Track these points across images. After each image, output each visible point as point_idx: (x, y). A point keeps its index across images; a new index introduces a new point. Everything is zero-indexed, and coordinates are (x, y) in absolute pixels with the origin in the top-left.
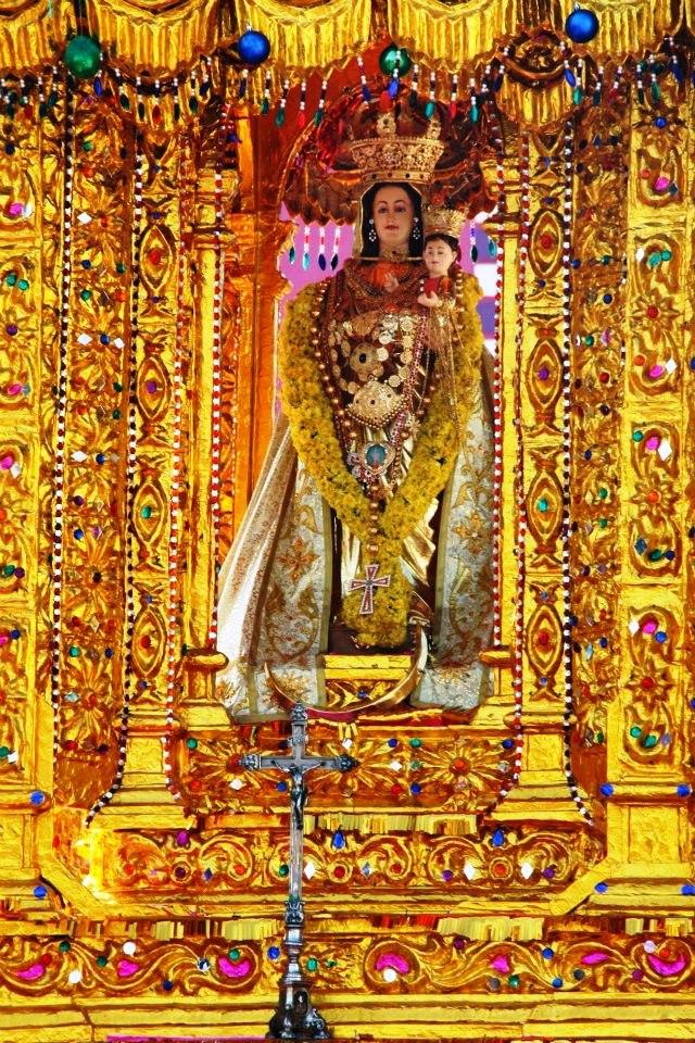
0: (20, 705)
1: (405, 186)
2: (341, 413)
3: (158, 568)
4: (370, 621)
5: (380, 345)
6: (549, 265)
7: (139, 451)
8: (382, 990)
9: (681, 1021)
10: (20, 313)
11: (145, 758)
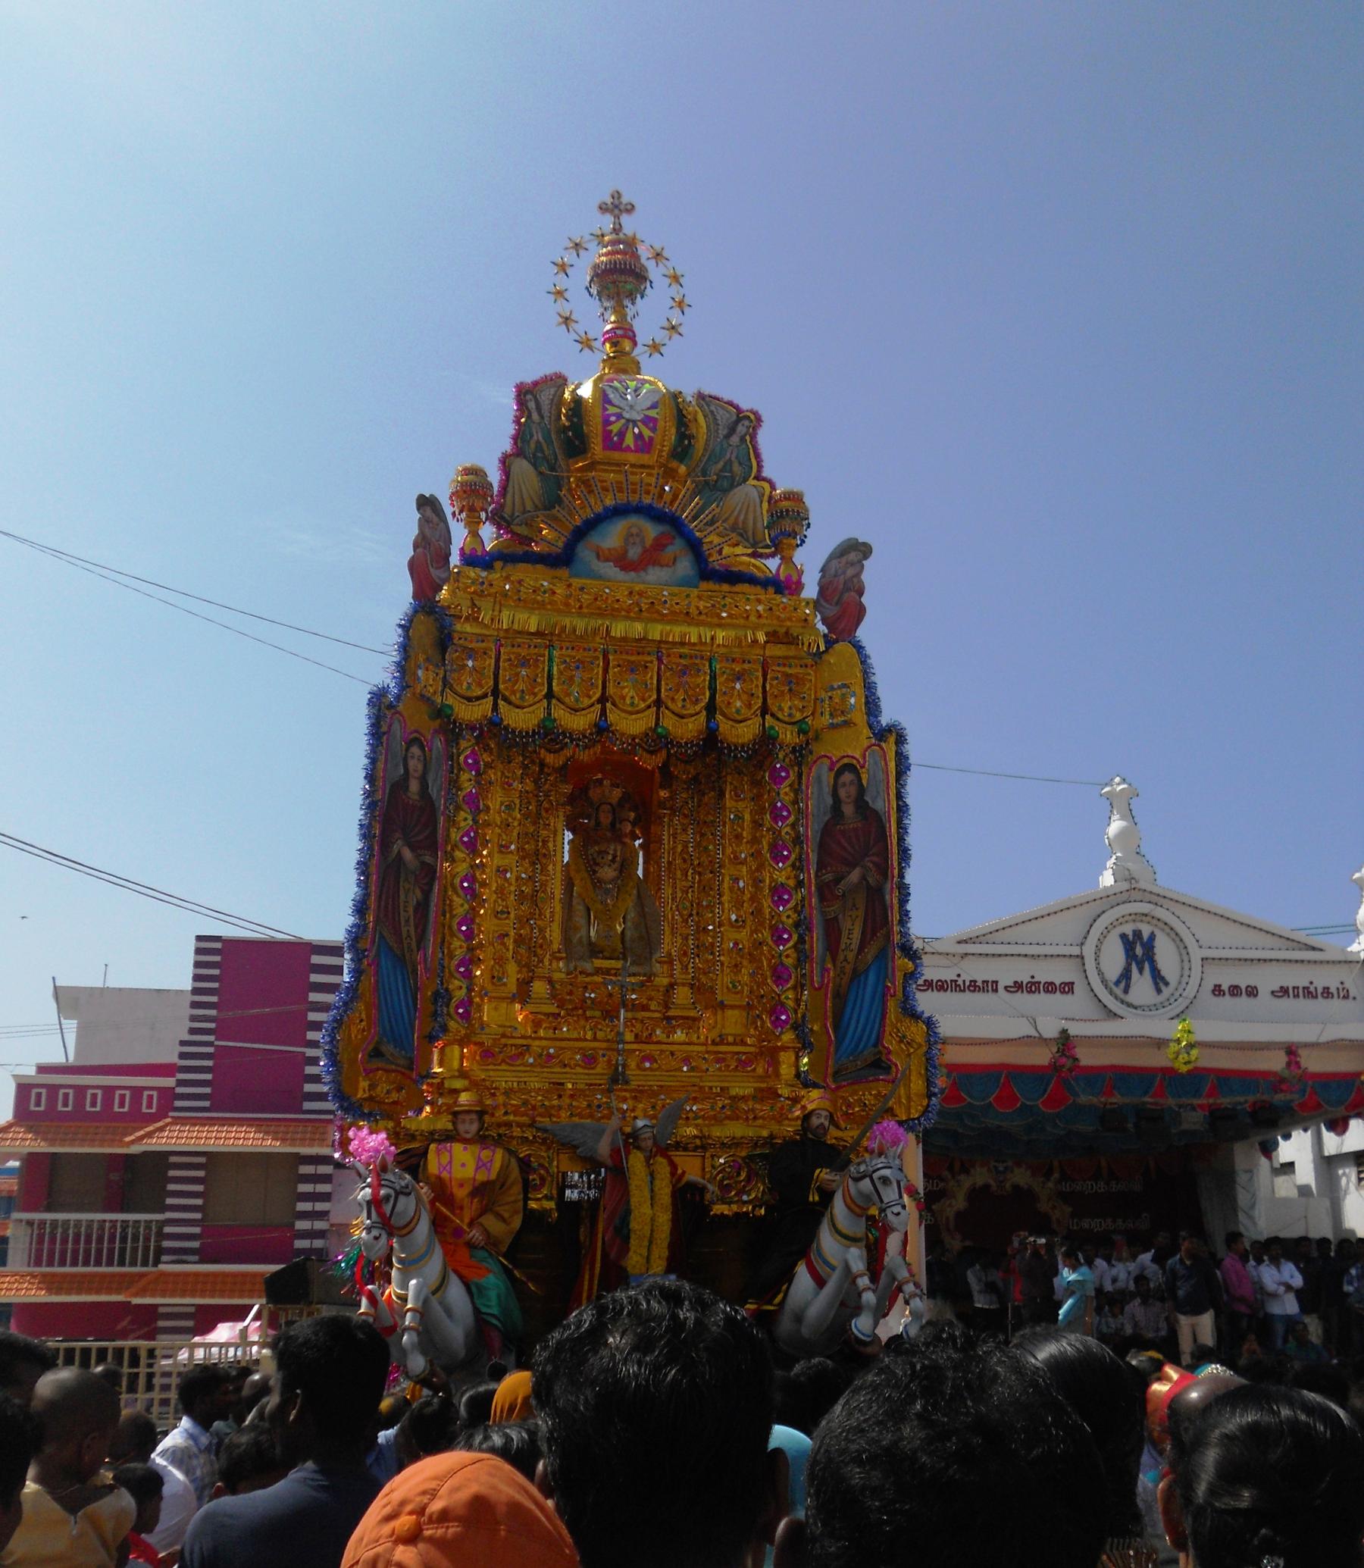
1: (610, 804)
8: (645, 1069)
9: (1018, 987)
10: (510, 820)
11: (539, 988)
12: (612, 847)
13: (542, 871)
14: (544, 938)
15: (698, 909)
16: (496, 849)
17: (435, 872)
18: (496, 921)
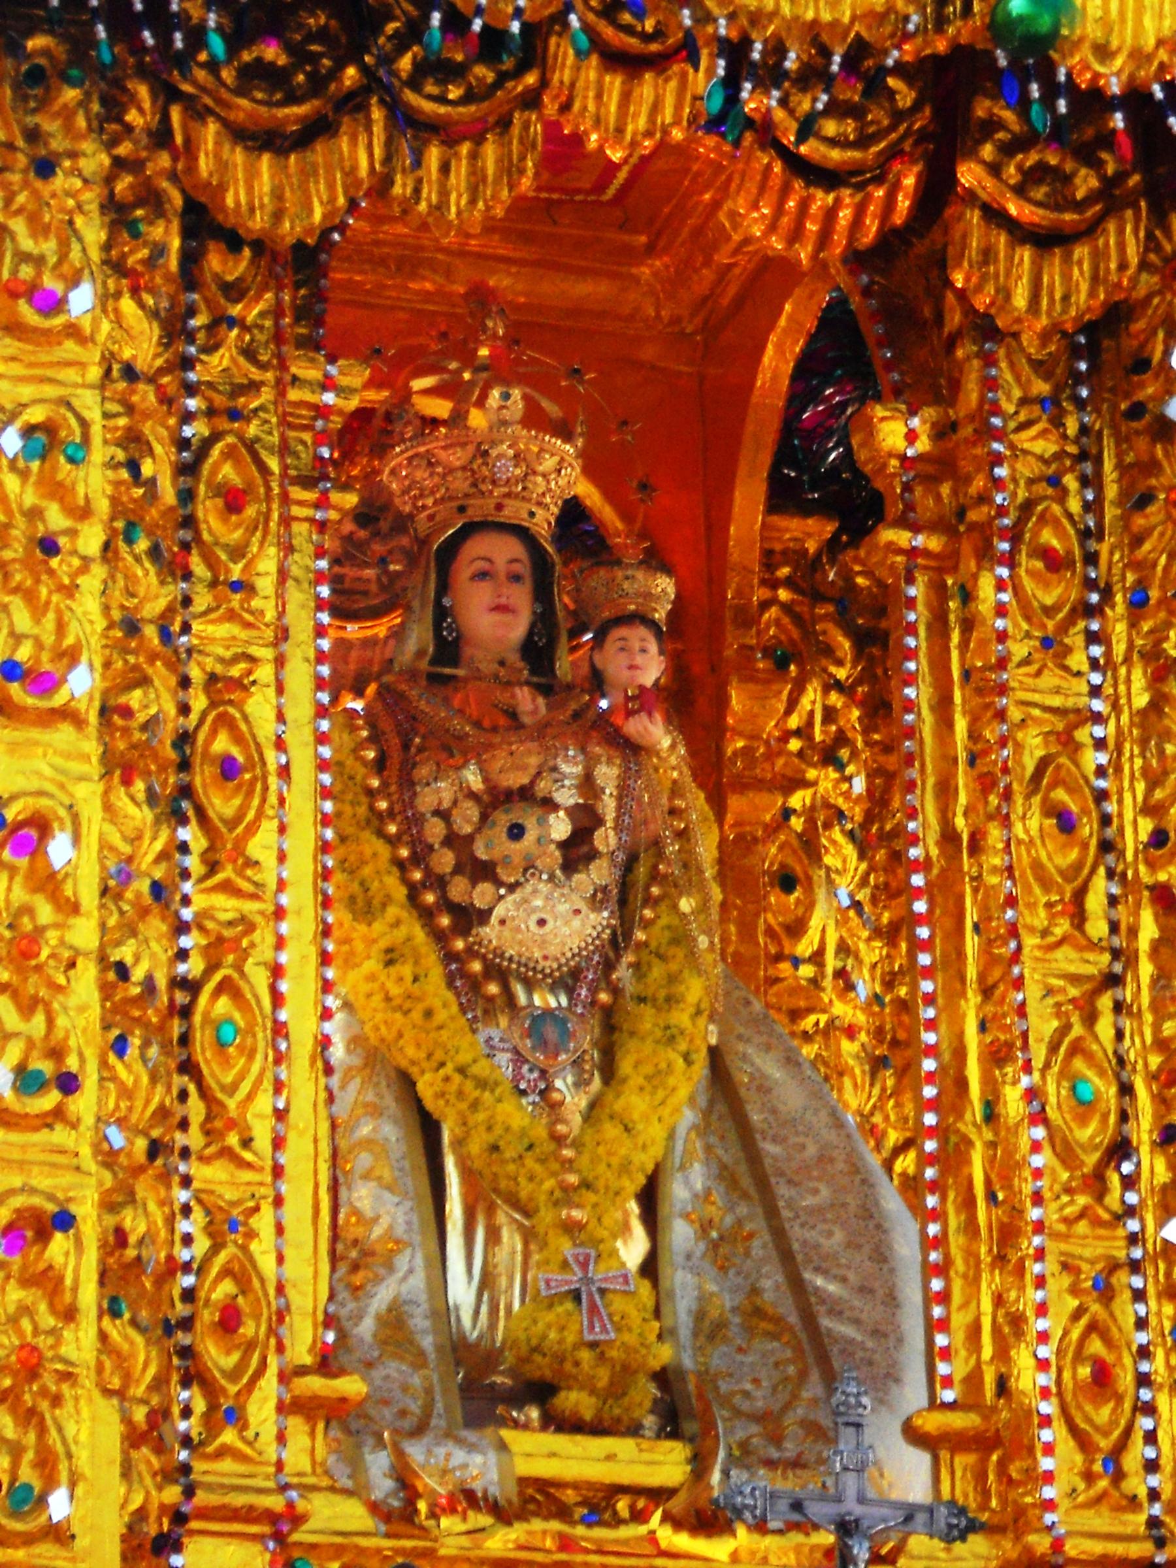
0: (65, 1388)
1: (522, 533)
2: (460, 945)
4: (602, 1357)
5: (555, 807)
6: (220, 990)
7: (200, 901)
12: (571, 769)
13: (212, 867)
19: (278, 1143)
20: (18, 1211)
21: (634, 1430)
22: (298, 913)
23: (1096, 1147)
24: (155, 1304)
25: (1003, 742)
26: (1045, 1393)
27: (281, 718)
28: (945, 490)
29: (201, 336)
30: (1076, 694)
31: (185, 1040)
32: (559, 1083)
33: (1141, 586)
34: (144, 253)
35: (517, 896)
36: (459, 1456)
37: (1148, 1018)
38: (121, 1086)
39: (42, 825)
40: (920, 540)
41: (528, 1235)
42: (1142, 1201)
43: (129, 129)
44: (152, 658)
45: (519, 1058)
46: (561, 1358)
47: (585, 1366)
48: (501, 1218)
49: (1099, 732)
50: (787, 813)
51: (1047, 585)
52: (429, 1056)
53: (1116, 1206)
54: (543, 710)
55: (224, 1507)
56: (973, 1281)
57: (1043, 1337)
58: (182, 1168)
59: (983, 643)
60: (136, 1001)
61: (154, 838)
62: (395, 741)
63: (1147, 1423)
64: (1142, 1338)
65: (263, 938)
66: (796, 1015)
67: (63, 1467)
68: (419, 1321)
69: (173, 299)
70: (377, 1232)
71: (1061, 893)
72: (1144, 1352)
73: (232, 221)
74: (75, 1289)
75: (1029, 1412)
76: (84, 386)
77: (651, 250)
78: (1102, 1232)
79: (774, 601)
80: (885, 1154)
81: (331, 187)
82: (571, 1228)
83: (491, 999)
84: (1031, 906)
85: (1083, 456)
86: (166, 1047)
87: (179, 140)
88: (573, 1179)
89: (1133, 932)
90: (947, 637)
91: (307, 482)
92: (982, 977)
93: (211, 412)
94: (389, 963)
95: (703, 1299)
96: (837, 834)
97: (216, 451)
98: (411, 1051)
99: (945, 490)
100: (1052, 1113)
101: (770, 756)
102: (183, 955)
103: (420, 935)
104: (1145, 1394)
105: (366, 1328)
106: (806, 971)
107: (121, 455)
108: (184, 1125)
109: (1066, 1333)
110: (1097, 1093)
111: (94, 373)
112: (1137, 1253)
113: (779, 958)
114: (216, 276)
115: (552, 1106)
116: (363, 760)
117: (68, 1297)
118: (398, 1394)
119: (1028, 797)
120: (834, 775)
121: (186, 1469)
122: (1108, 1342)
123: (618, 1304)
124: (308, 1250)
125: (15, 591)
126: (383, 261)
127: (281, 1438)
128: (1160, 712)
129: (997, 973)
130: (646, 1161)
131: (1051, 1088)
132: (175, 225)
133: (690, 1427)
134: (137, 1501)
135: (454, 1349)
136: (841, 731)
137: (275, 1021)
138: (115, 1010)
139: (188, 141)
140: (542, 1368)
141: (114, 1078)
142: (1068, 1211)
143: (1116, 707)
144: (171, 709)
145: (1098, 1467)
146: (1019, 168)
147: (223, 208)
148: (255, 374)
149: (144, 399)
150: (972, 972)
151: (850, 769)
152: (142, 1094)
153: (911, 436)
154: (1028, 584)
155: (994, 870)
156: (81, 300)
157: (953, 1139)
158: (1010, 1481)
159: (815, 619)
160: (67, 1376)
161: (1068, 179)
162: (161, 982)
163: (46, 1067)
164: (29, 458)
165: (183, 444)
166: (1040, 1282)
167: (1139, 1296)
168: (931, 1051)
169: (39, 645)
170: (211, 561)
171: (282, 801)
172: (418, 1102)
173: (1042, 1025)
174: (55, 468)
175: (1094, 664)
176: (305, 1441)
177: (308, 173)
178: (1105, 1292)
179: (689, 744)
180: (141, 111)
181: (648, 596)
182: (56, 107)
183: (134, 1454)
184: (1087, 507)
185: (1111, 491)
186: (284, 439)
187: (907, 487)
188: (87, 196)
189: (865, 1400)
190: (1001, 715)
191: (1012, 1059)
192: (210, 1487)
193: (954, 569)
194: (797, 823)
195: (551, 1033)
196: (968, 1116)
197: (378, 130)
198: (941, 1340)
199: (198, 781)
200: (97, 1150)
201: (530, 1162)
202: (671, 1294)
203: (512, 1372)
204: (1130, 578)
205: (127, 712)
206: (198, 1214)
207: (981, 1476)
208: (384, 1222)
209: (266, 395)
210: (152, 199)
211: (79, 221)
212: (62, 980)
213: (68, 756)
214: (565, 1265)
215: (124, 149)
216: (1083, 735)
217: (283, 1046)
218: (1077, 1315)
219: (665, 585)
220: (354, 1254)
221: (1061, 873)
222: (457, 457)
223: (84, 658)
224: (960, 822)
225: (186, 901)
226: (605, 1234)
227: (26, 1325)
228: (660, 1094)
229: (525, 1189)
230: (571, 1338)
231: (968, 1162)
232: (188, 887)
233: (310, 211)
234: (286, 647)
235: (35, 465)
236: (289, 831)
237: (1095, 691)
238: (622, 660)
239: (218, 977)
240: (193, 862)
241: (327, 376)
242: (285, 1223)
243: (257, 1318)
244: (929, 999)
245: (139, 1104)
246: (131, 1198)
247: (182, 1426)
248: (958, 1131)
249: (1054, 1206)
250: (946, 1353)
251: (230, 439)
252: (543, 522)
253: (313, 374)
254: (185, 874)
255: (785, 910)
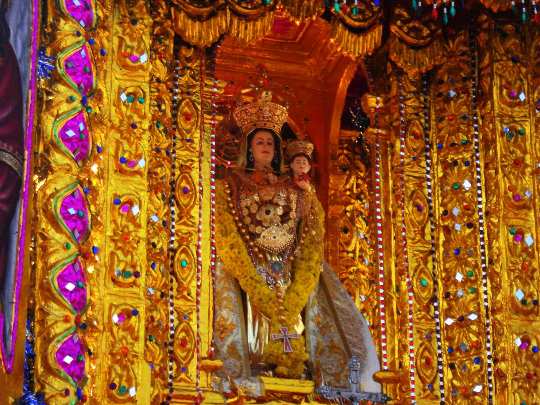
0: (135, 359)
2: (252, 244)
3: (189, 298)
6: (182, 252)
7: (177, 227)
10: (136, 119)
13: (181, 218)
14: (187, 330)
15: (446, 286)
16: (112, 165)
17: (20, 180)
18: (116, 289)
19: (198, 294)
20: (122, 310)
21: (299, 378)
22: (205, 232)
23: (427, 298)
24: (162, 338)
25: (402, 186)
26: (412, 366)
27: (200, 177)
28: (387, 118)
29: (180, 72)
30: (422, 173)
31: (172, 265)
32: (279, 282)
33: (441, 143)
34: (163, 48)
35: (268, 230)
36: (249, 383)
37: (442, 263)
38: (153, 277)
39: (130, 203)
40: (380, 131)
41: (270, 324)
42: (440, 313)
43: (159, 13)
44: (164, 159)
45: (268, 274)
46: (277, 357)
47: (284, 359)
48: (263, 319)
49: (429, 183)
50: (346, 211)
51: (415, 143)
52: (243, 274)
53: (433, 315)
54: (276, 179)
55: (181, 395)
56: (393, 337)
57: (412, 351)
58: (171, 301)
59: (397, 159)
60: (158, 254)
61: (164, 209)
62: (235, 188)
63: (441, 375)
64: (440, 352)
65: (195, 238)
66: (348, 267)
67: (134, 381)
68: (239, 347)
69: (171, 61)
70: (228, 323)
71: (418, 228)
72: (440, 356)
73: (187, 40)
74: (138, 332)
75: (408, 372)
76: (145, 82)
77: (309, 57)
78: (429, 322)
79: (343, 153)
80: (373, 307)
81: (215, 31)
82: (281, 322)
83: (260, 258)
84: (410, 232)
85: (425, 107)
86: (166, 267)
87: (173, 17)
88: (282, 308)
89: (438, 239)
90: (387, 158)
91: (209, 113)
92: (396, 252)
93: (182, 93)
94: (232, 248)
95: (318, 343)
96: (360, 218)
97: (183, 104)
98: (238, 273)
99: (387, 118)
100: (415, 289)
101: (341, 196)
102: (172, 242)
103: (240, 240)
104: (440, 367)
105: (225, 349)
106: (351, 255)
107: (156, 103)
108: (172, 289)
109: (418, 350)
110: (427, 284)
111: (147, 79)
112: (438, 328)
113: (344, 251)
114: (184, 56)
115: (277, 288)
116: (226, 193)
117: (136, 334)
118: (233, 367)
119: (409, 201)
120: (360, 202)
121: (171, 384)
122: (430, 352)
123: (294, 342)
124: (207, 325)
125: (125, 138)
126: (235, 59)
127: (198, 377)
128: (446, 178)
129: (400, 250)
130: (303, 303)
131: (415, 282)
132: (172, 41)
133: (314, 377)
134: (156, 392)
135: (249, 355)
136: (362, 190)
137: (198, 261)
138: (152, 256)
139: (176, 17)
140: (272, 360)
141: (151, 275)
142: (419, 316)
143: (434, 177)
144: (169, 173)
145: (427, 387)
146: (408, 27)
147: (185, 36)
148: (195, 82)
149: (163, 88)
150: (393, 251)
151: (364, 201)
152: (159, 279)
153: (377, 102)
154: (409, 143)
155: (400, 222)
156: (144, 58)
157: (388, 296)
158: (403, 392)
159: (355, 159)
160: (136, 356)
161: (421, 30)
162: (165, 249)
163: (131, 270)
164: (128, 102)
165: (174, 101)
166: (411, 336)
167: (439, 340)
168: (382, 272)
169: (130, 153)
170: (181, 134)
171: (200, 200)
172: (240, 287)
173: (412, 264)
174: (136, 105)
175: (428, 165)
176: (206, 378)
177: (209, 27)
178: (429, 338)
179: (316, 190)
180: (163, 9)
181: (306, 148)
182: (138, 6)
183: (156, 380)
184: (426, 121)
185: (433, 117)
186: (202, 101)
187: (376, 116)
188: (146, 30)
189: (358, 364)
190: (402, 179)
191: (403, 274)
192: (177, 390)
193: (389, 140)
194: (348, 214)
195: (277, 268)
196: (392, 290)
197: (229, 15)
198: (384, 352)
199: (177, 194)
200: (145, 295)
201: (270, 303)
202: (309, 342)
203: (265, 362)
204: (438, 141)
205: (156, 174)
206: (175, 314)
207: (394, 390)
208: (230, 320)
209: (198, 89)
210: (165, 33)
211: (144, 37)
212: (136, 246)
213: (139, 184)
214: (280, 332)
215: (158, 19)
216: (424, 184)
217: (200, 268)
218: (421, 345)
219: (310, 146)
220: (222, 329)
221: (418, 222)
222: (253, 111)
223: (143, 157)
224: (390, 209)
225: (173, 227)
226: (291, 323)
227: (124, 341)
228: (307, 285)
229: (269, 311)
230: (280, 352)
231: (392, 303)
232: (174, 223)
233: (209, 37)
234: (202, 158)
235: (130, 104)
236: (203, 209)
237: (428, 172)
238: (299, 166)
239: (182, 248)
240: (175, 217)
241: (215, 84)
242: (200, 317)
243: (191, 343)
244: (381, 258)
245: (158, 282)
246: (156, 309)
247: (170, 372)
248: (389, 295)
249: (415, 315)
250: (385, 356)
251: (187, 100)
252: (277, 129)
253: (211, 83)
254: (173, 220)
255: (345, 238)
